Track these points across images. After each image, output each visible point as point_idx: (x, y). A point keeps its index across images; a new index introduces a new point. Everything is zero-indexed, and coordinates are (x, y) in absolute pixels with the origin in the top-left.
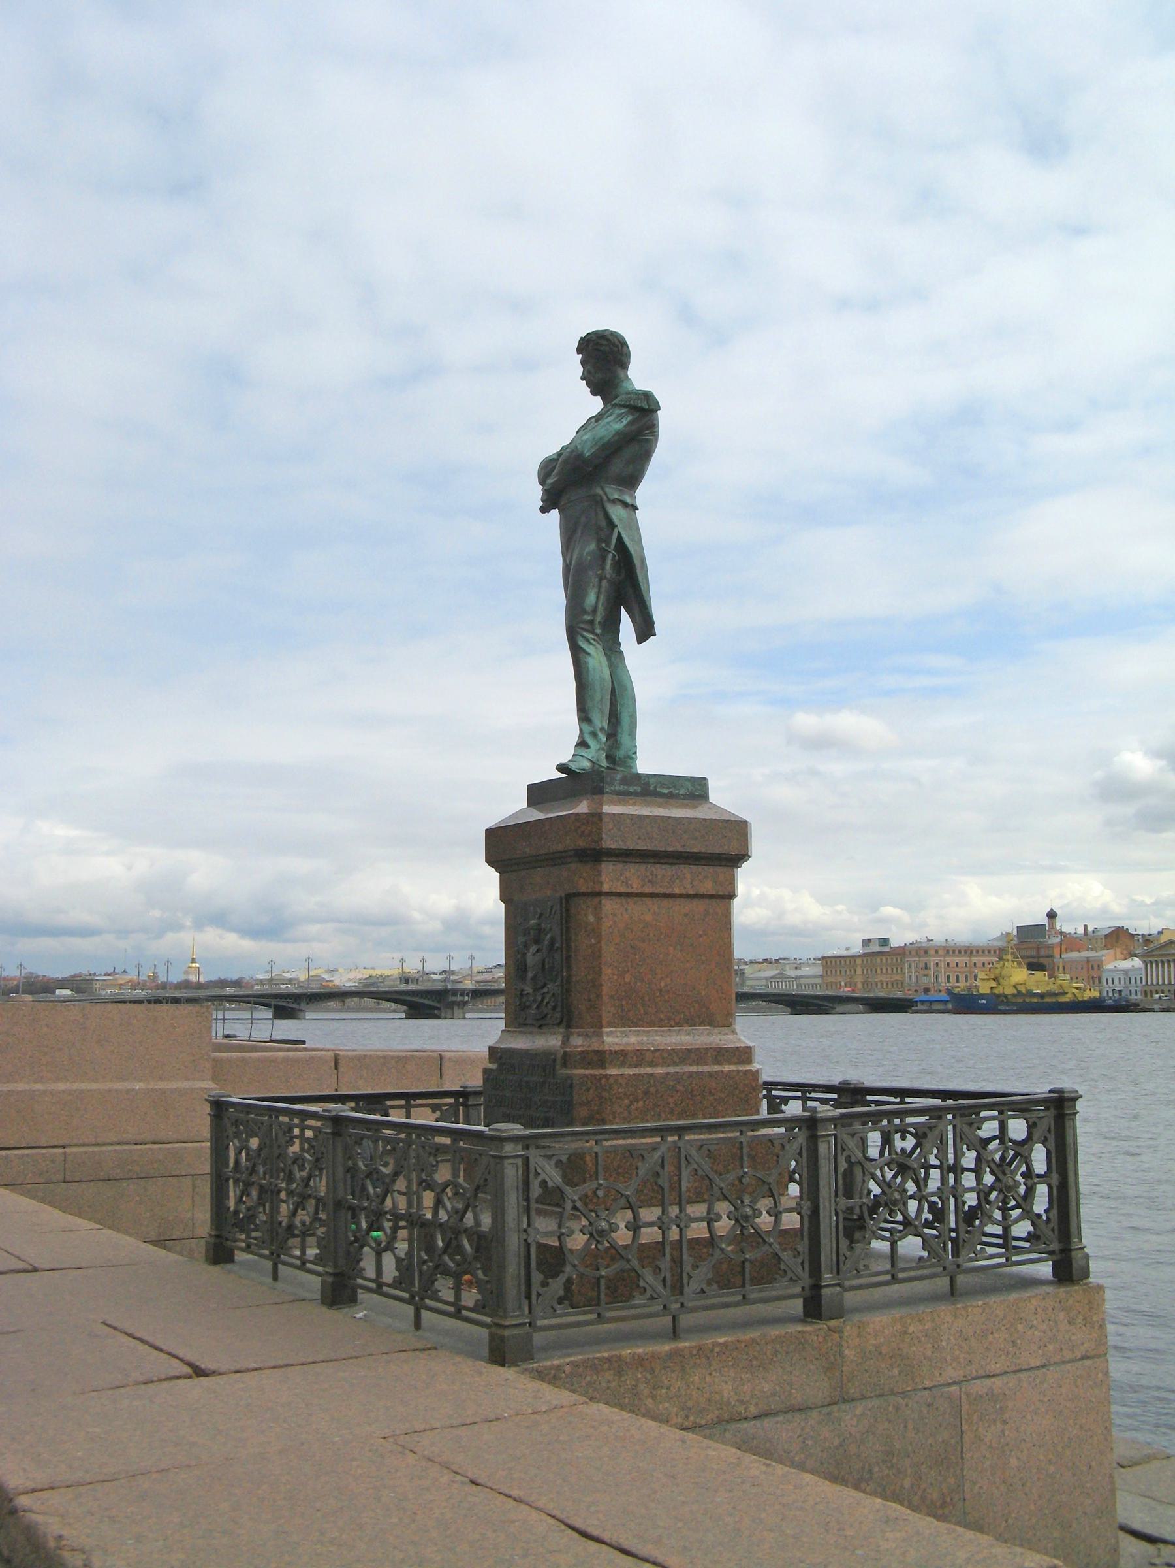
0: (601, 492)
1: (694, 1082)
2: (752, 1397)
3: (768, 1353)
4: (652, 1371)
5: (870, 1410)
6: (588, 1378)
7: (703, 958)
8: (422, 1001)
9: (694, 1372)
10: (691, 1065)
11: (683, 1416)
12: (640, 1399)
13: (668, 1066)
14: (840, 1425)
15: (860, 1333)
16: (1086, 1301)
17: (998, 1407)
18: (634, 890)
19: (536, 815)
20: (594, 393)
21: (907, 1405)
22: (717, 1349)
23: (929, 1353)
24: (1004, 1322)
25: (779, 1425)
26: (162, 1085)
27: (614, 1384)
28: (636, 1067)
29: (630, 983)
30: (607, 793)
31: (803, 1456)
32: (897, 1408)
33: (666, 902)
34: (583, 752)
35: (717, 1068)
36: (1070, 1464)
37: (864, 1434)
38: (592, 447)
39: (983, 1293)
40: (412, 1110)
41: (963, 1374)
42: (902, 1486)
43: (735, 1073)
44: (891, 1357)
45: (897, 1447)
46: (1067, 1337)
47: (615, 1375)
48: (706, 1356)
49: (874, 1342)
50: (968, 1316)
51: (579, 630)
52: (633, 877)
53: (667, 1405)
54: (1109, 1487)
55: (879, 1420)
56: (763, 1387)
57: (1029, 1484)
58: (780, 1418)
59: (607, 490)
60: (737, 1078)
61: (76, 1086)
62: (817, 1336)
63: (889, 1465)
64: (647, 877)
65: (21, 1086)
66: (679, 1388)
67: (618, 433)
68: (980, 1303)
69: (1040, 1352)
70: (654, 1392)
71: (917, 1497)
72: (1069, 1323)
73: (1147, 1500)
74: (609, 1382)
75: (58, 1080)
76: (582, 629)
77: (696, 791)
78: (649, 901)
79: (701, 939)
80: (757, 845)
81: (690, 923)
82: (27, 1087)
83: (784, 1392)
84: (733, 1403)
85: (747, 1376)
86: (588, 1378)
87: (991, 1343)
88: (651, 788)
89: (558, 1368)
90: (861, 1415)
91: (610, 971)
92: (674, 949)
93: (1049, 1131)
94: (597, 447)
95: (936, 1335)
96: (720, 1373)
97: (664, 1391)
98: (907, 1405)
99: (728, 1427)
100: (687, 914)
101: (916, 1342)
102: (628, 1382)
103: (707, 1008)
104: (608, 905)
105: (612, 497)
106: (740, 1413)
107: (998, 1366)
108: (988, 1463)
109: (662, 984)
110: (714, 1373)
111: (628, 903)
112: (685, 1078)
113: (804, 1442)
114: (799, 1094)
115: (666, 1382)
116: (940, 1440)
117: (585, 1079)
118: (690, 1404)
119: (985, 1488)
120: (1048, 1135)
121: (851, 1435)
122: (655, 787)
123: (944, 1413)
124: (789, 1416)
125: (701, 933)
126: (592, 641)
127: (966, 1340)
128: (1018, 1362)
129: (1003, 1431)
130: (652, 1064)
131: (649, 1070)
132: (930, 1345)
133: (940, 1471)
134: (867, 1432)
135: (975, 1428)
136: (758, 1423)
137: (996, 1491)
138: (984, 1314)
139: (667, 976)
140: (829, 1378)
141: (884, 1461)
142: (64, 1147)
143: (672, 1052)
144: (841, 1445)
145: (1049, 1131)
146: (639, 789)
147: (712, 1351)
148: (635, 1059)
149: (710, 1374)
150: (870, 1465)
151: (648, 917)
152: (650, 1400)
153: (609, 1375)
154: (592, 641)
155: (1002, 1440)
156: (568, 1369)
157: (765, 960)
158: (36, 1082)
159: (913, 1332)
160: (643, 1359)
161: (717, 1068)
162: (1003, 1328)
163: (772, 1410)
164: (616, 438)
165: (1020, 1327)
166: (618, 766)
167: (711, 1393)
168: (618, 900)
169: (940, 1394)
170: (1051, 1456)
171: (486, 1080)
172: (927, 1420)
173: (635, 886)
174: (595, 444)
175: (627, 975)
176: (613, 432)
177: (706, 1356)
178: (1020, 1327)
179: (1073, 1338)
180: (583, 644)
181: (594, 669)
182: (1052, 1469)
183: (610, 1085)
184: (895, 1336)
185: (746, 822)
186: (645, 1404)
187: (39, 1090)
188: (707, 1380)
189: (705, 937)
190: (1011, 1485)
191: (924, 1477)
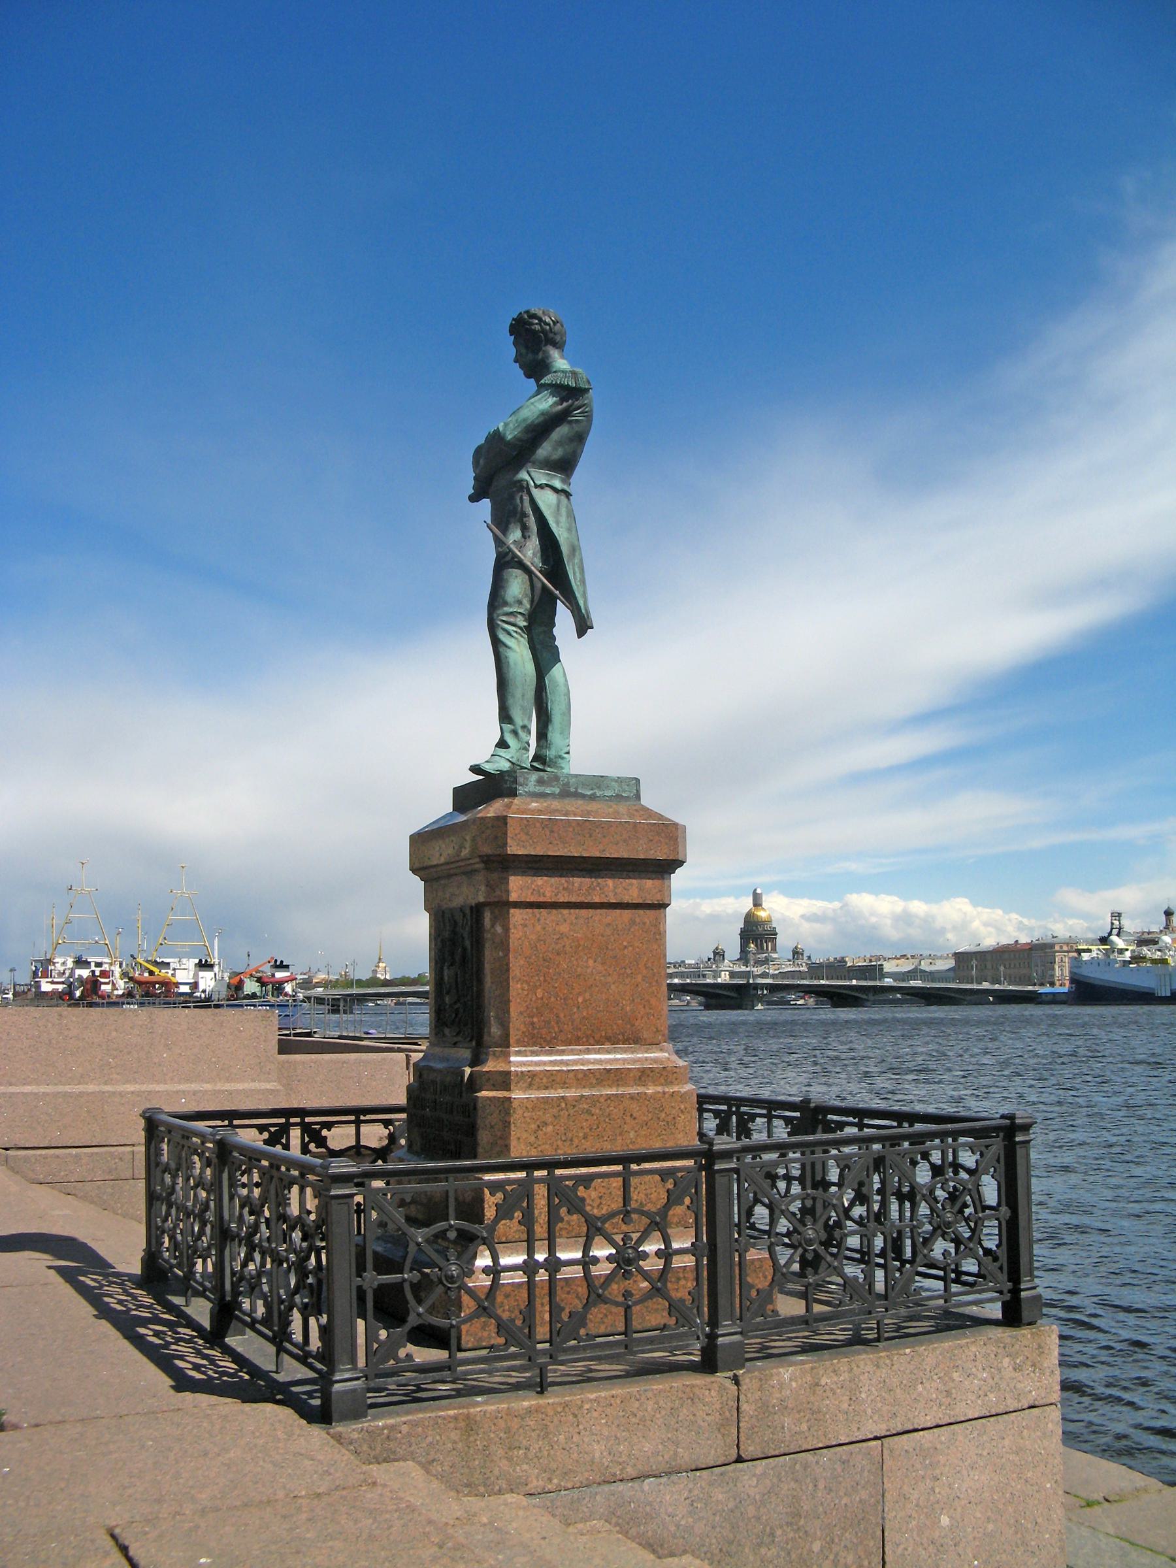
0: (527, 477)
3: (649, 1409)
5: (772, 1469)
6: (430, 1439)
8: (720, 992)
10: (610, 1086)
11: (546, 1479)
12: (492, 1461)
13: (584, 1087)
14: (736, 1486)
15: (761, 1386)
16: (1035, 1346)
17: (927, 1462)
19: (462, 818)
20: (528, 376)
21: (817, 1462)
22: (587, 1406)
23: (845, 1406)
25: (662, 1487)
26: (228, 1086)
27: (460, 1445)
28: (547, 1088)
29: (542, 999)
30: (520, 794)
31: (690, 1520)
32: (806, 1467)
34: (501, 752)
35: (640, 1089)
36: (1012, 1521)
37: (764, 1495)
41: (886, 1428)
42: (811, 1551)
43: (660, 1095)
44: (799, 1412)
46: (1012, 1385)
48: (573, 1414)
49: (778, 1395)
51: (499, 623)
52: (547, 887)
53: (525, 1467)
54: (1058, 1544)
57: (962, 1545)
58: (663, 1480)
59: (533, 474)
60: (663, 1100)
61: (144, 1088)
63: (795, 1527)
65: (91, 1088)
66: (540, 1448)
67: (543, 414)
68: (908, 1351)
69: (979, 1402)
70: (511, 1453)
71: (827, 1562)
72: (1015, 1369)
73: (1123, 1543)
74: (455, 1442)
75: (128, 1082)
76: (503, 621)
79: (626, 952)
80: (693, 853)
82: (97, 1089)
84: (606, 1464)
86: (430, 1439)
87: (920, 1394)
89: (392, 1428)
90: (761, 1474)
91: (519, 986)
94: (519, 430)
98: (817, 1462)
99: (600, 1489)
100: (609, 924)
101: (829, 1394)
103: (633, 1025)
105: (538, 483)
106: (614, 1475)
107: (928, 1418)
108: (914, 1523)
109: (580, 1000)
110: (583, 1432)
112: (602, 1100)
114: (764, 1112)
115: (524, 1442)
116: (858, 1499)
117: (488, 1102)
118: (554, 1466)
119: (910, 1549)
121: (749, 1496)
122: (576, 788)
123: (863, 1470)
124: (674, 1477)
125: (625, 943)
126: (514, 634)
128: (952, 1413)
129: (933, 1489)
130: (565, 1085)
131: (561, 1093)
133: (856, 1533)
134: (769, 1492)
136: (636, 1484)
137: (924, 1552)
140: (723, 1435)
141: (789, 1524)
142: (133, 1145)
144: (736, 1507)
147: (581, 1407)
150: (771, 1528)
151: (564, 928)
152: (504, 1462)
153: (454, 1435)
154: (514, 634)
155: (932, 1498)
156: (405, 1429)
157: (904, 956)
158: (106, 1083)
161: (640, 1089)
162: (935, 1377)
163: (653, 1471)
164: (541, 419)
165: (955, 1375)
166: (549, 766)
170: (989, 1514)
171: (409, 1099)
172: (841, 1479)
173: (548, 894)
178: (955, 1375)
179: (1019, 1386)
180: (503, 637)
181: (515, 664)
182: (990, 1527)
185: (676, 825)
186: (499, 1467)
187: (108, 1092)
188: (574, 1439)
189: (630, 948)
190: (942, 1546)
191: (836, 1540)
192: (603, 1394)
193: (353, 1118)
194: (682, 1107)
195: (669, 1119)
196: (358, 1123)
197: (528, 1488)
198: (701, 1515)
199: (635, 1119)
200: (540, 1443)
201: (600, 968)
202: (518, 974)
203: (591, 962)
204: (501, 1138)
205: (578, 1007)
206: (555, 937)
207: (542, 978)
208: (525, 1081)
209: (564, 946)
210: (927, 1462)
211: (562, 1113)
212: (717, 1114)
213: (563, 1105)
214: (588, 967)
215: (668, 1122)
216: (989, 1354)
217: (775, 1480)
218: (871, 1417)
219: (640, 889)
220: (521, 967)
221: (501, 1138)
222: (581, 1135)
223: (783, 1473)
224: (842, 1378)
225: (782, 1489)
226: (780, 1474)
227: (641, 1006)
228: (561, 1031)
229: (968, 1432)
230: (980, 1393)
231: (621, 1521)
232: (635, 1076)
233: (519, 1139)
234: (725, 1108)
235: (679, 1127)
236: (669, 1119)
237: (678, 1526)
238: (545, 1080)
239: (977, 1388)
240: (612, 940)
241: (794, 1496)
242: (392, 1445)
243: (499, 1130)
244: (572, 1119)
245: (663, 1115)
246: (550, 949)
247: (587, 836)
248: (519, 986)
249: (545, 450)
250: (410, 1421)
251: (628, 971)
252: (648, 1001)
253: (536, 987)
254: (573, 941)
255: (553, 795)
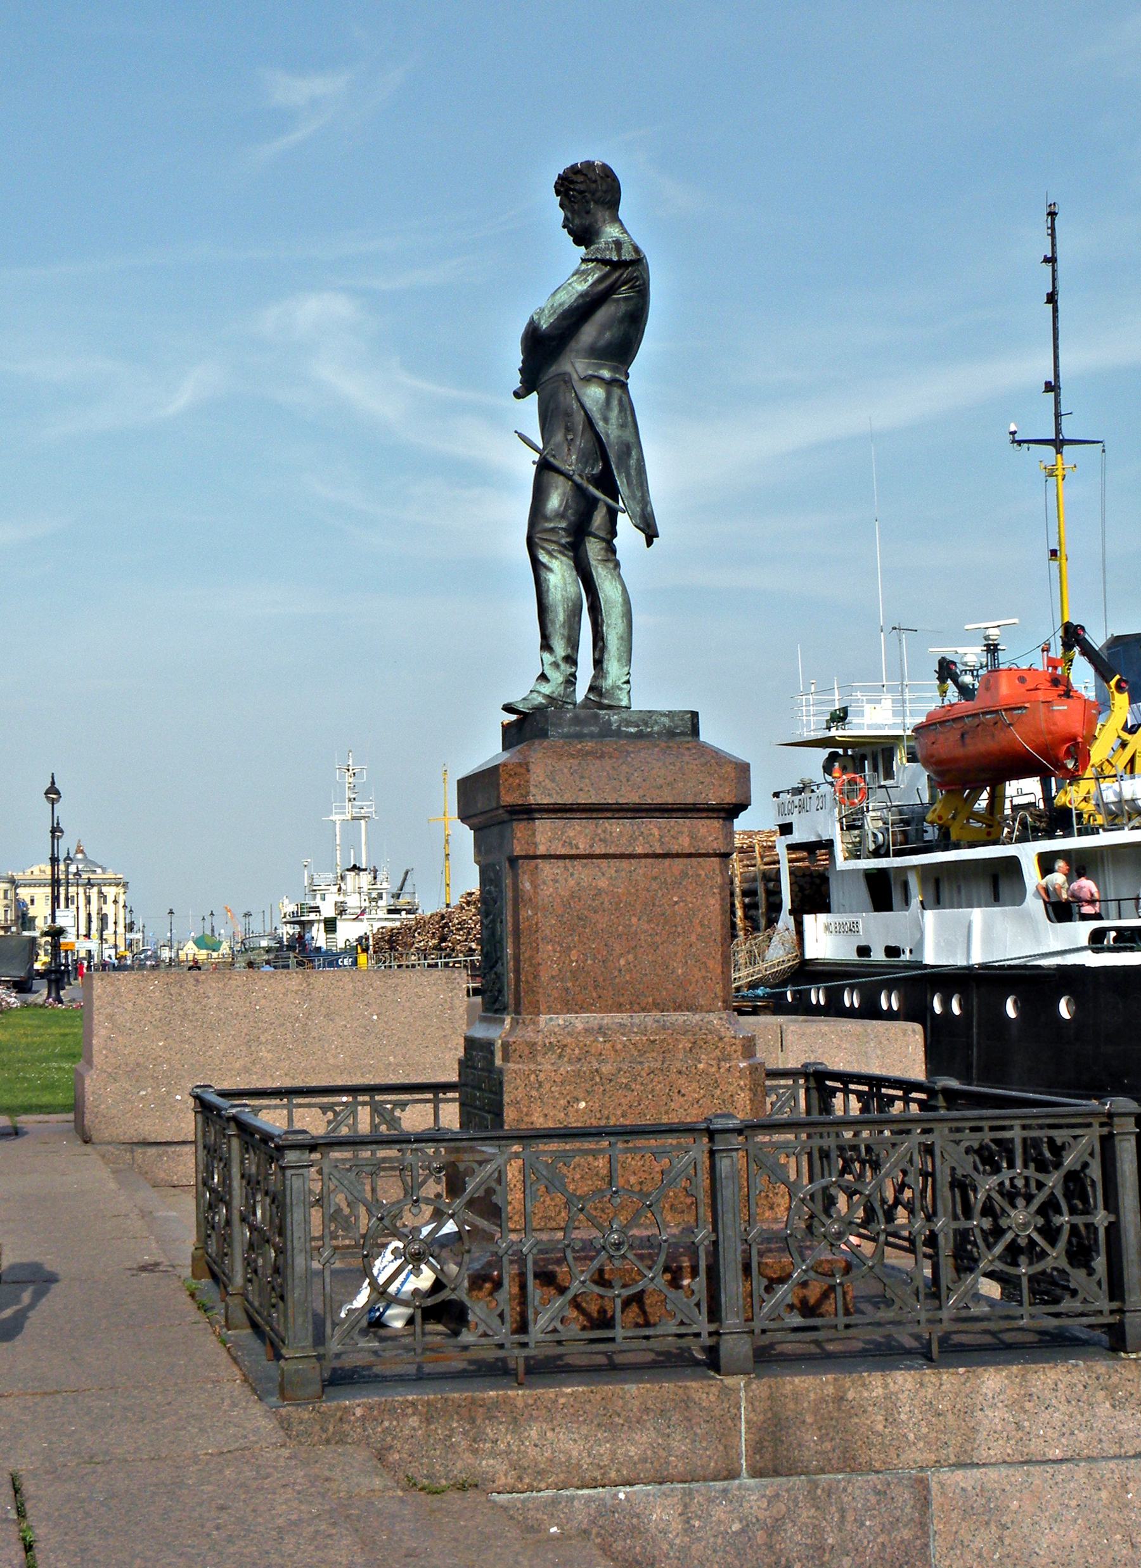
1: (656, 1080)
2: (612, 1461)
4: (473, 1421)
6: (386, 1424)
7: (679, 929)
9: (530, 1426)
14: (741, 1506)
17: (992, 1506)
18: (581, 851)
22: (562, 1400)
24: (1001, 1397)
33: (624, 864)
38: (550, 316)
39: (928, 1358)
40: (441, 1105)
45: (830, 1541)
47: (421, 1422)
50: (941, 1385)
53: (491, 1462)
55: (800, 1505)
56: (629, 1451)
62: (707, 1393)
64: (599, 835)
67: (582, 295)
74: (414, 1429)
77: (676, 728)
78: (604, 863)
81: (660, 888)
83: (658, 1459)
84: (585, 1466)
85: (606, 1434)
86: (386, 1424)
88: (613, 728)
90: (772, 1496)
91: (550, 947)
92: (639, 920)
93: (1092, 1154)
94: (555, 316)
95: (890, 1405)
96: (567, 1428)
97: (488, 1445)
102: (440, 1431)
104: (548, 870)
106: (595, 1479)
107: (992, 1452)
109: (622, 962)
111: (573, 867)
112: (644, 1074)
113: (688, 1522)
116: (899, 1539)
120: (1089, 1159)
121: (758, 1520)
122: (619, 726)
125: (675, 899)
127: (939, 1415)
129: (1000, 1539)
132: (880, 1418)
135: (954, 1529)
138: (968, 1385)
139: (628, 952)
143: (627, 1043)
145: (1092, 1154)
146: (595, 729)
148: (577, 1051)
149: (553, 1430)
151: (603, 883)
159: (854, 1399)
160: (459, 1406)
166: (606, 698)
167: (553, 1452)
168: (561, 863)
169: (895, 1481)
173: (581, 846)
174: (553, 314)
175: (573, 952)
176: (576, 295)
177: (546, 1407)
180: (543, 557)
183: (541, 1082)
184: (827, 1402)
189: (682, 904)
192: (580, 1389)
193: (430, 1096)
194: (742, 1083)
195: (726, 1096)
196: (436, 1102)
197: (495, 1485)
198: (699, 1535)
199: (683, 1095)
200: (509, 1437)
201: (645, 927)
202: (549, 934)
203: (634, 920)
204: (527, 1115)
205: (620, 971)
206: (592, 893)
207: (576, 938)
208: (554, 1052)
209: (602, 903)
210: (992, 1506)
211: (596, 1088)
212: (860, 1095)
213: (598, 1079)
214: (630, 926)
215: (724, 1101)
216: (1075, 1385)
217: (791, 1504)
218: (914, 1444)
219: (692, 837)
220: (552, 926)
221: (527, 1115)
222: (619, 1113)
223: (801, 1498)
224: (874, 1394)
225: (799, 1516)
226: (797, 1498)
227: (695, 969)
228: (600, 997)
229: (1049, 1475)
230: (1064, 1430)
231: (603, 1532)
232: (684, 1048)
233: (546, 1115)
234: (866, 1088)
235: (738, 1106)
236: (726, 1096)
237: (671, 1545)
238: (577, 1051)
239: (1060, 1424)
240: (660, 895)
241: (815, 1527)
242: (346, 1427)
243: (524, 1106)
244: (608, 1095)
245: (718, 1092)
246: (587, 906)
247: (624, 780)
248: (550, 947)
249: (589, 334)
250: (364, 1404)
251: (679, 929)
252: (704, 963)
253: (569, 949)
254: (614, 898)
255: (592, 736)
